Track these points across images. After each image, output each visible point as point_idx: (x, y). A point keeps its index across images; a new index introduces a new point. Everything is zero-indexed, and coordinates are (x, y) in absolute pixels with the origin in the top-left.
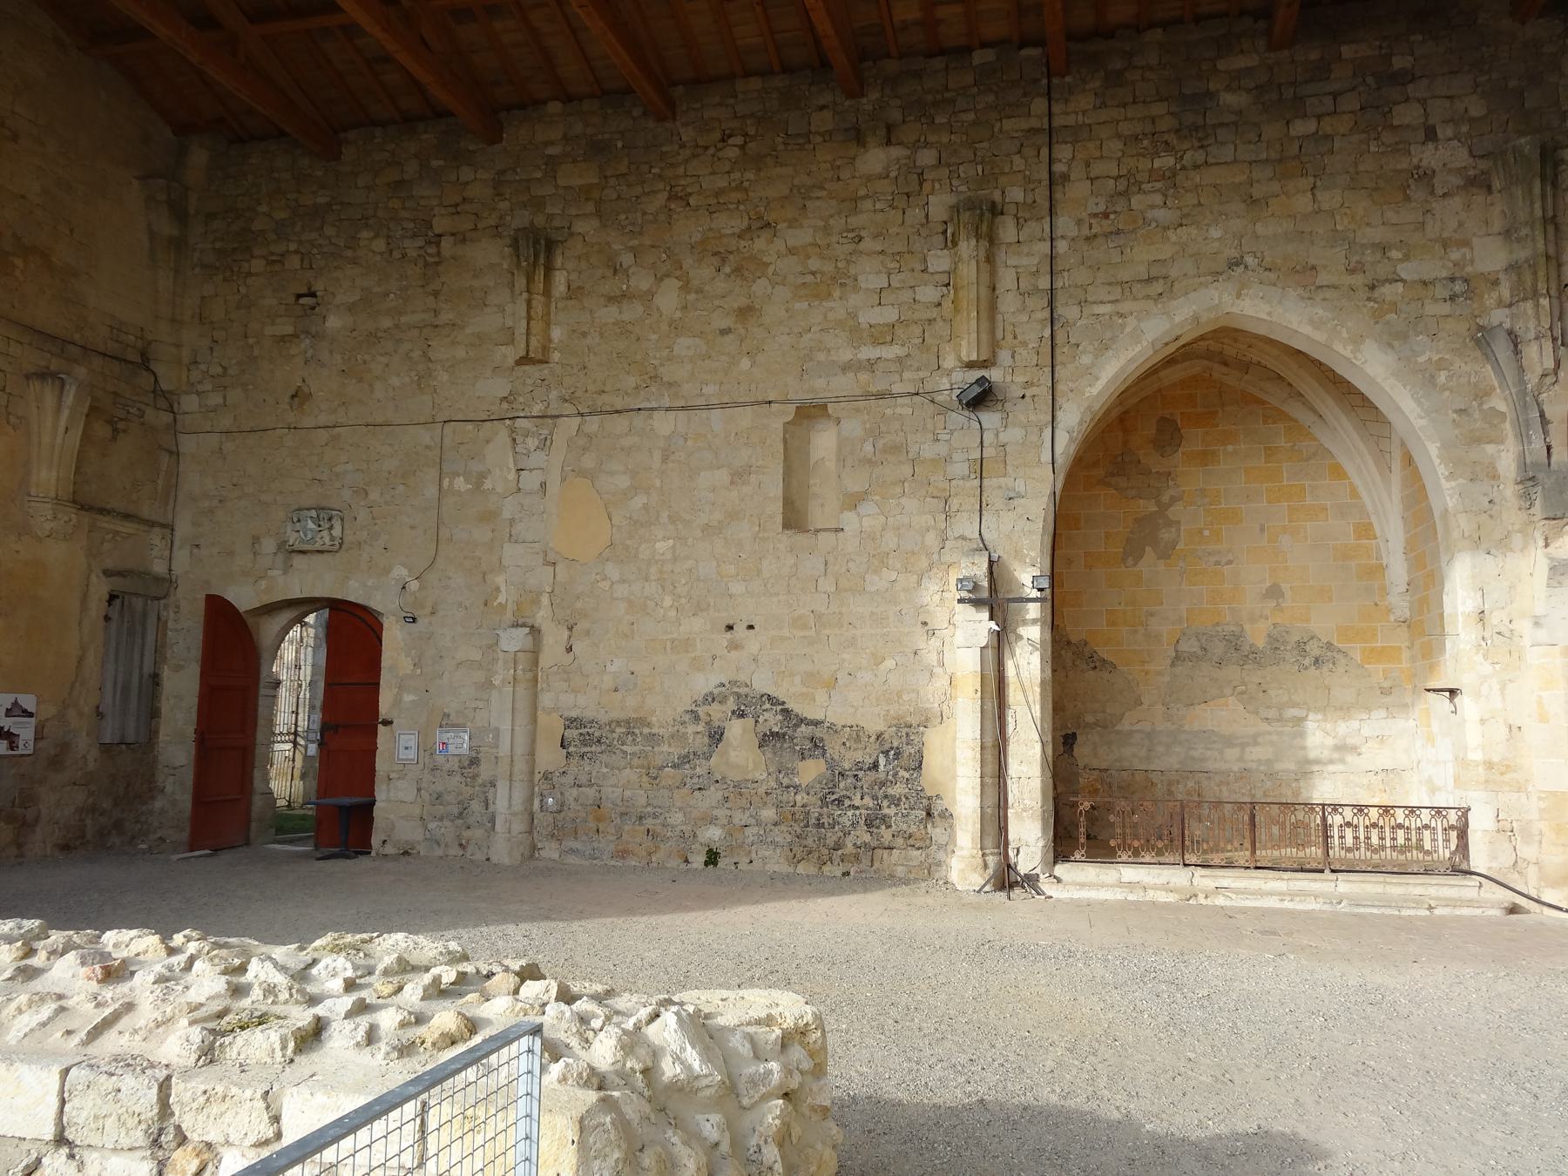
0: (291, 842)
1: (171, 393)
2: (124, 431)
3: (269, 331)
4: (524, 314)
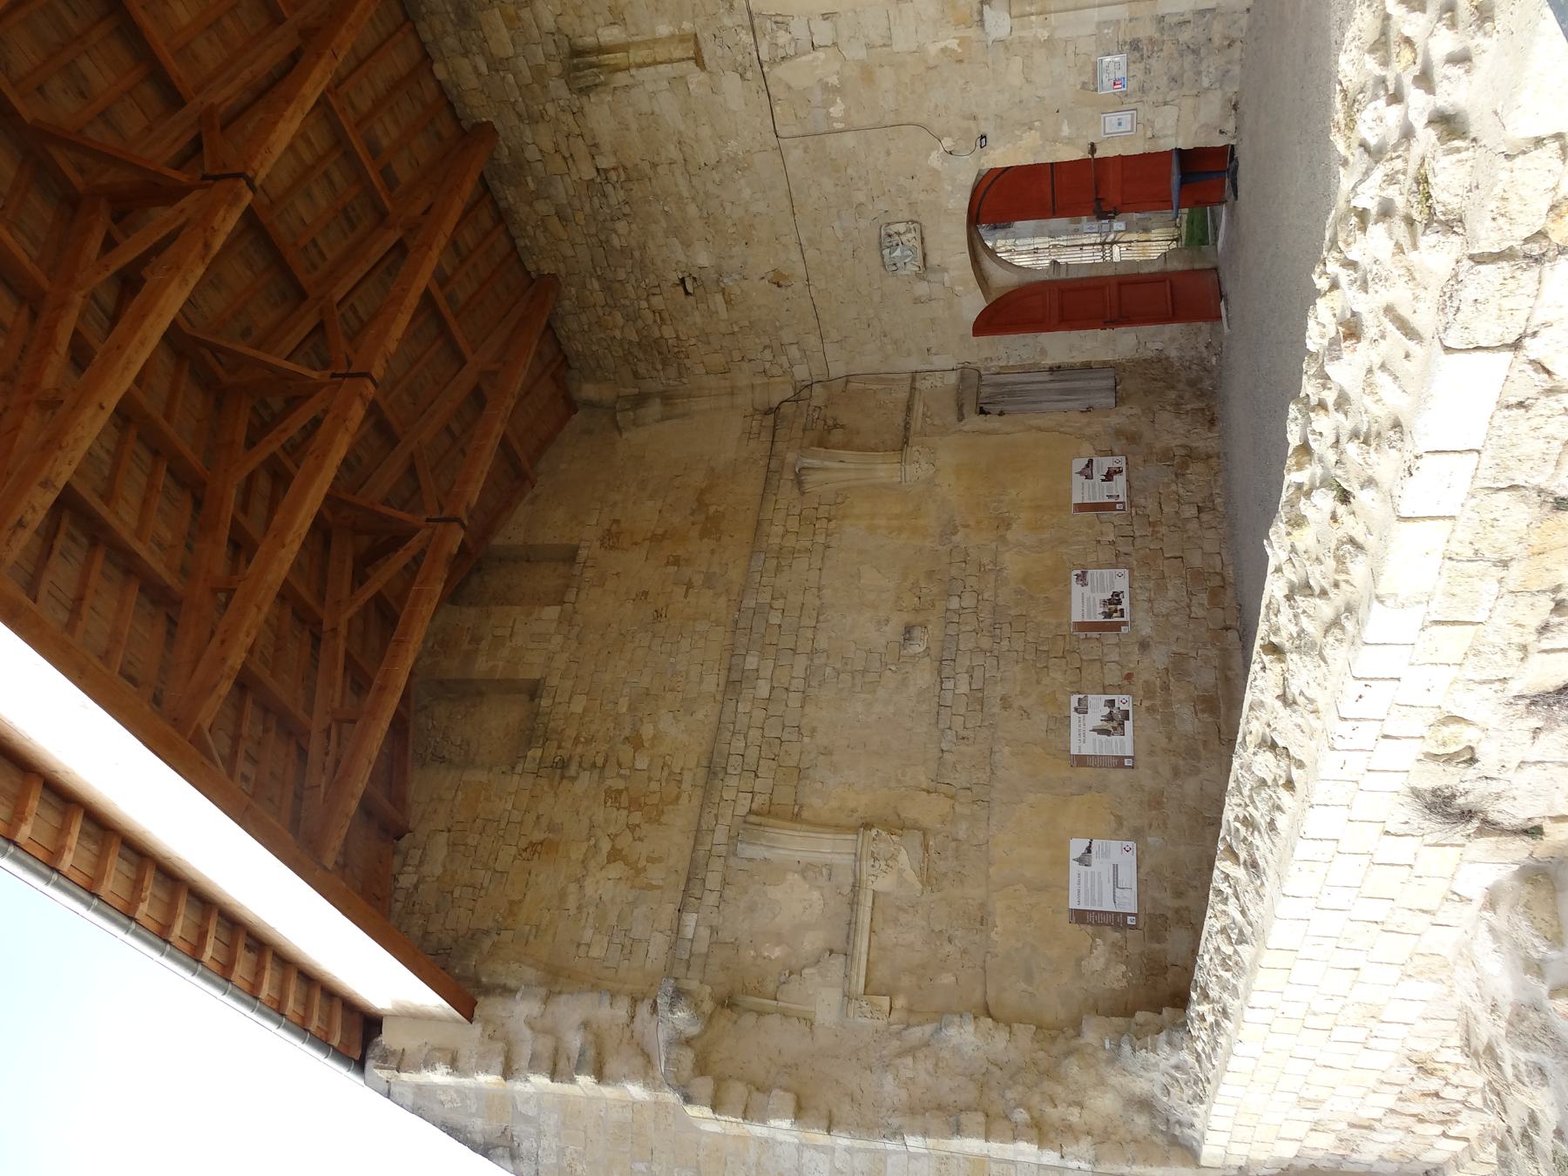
0: (1216, 229)
1: (795, 389)
2: (835, 420)
3: (724, 314)
4: (652, 70)
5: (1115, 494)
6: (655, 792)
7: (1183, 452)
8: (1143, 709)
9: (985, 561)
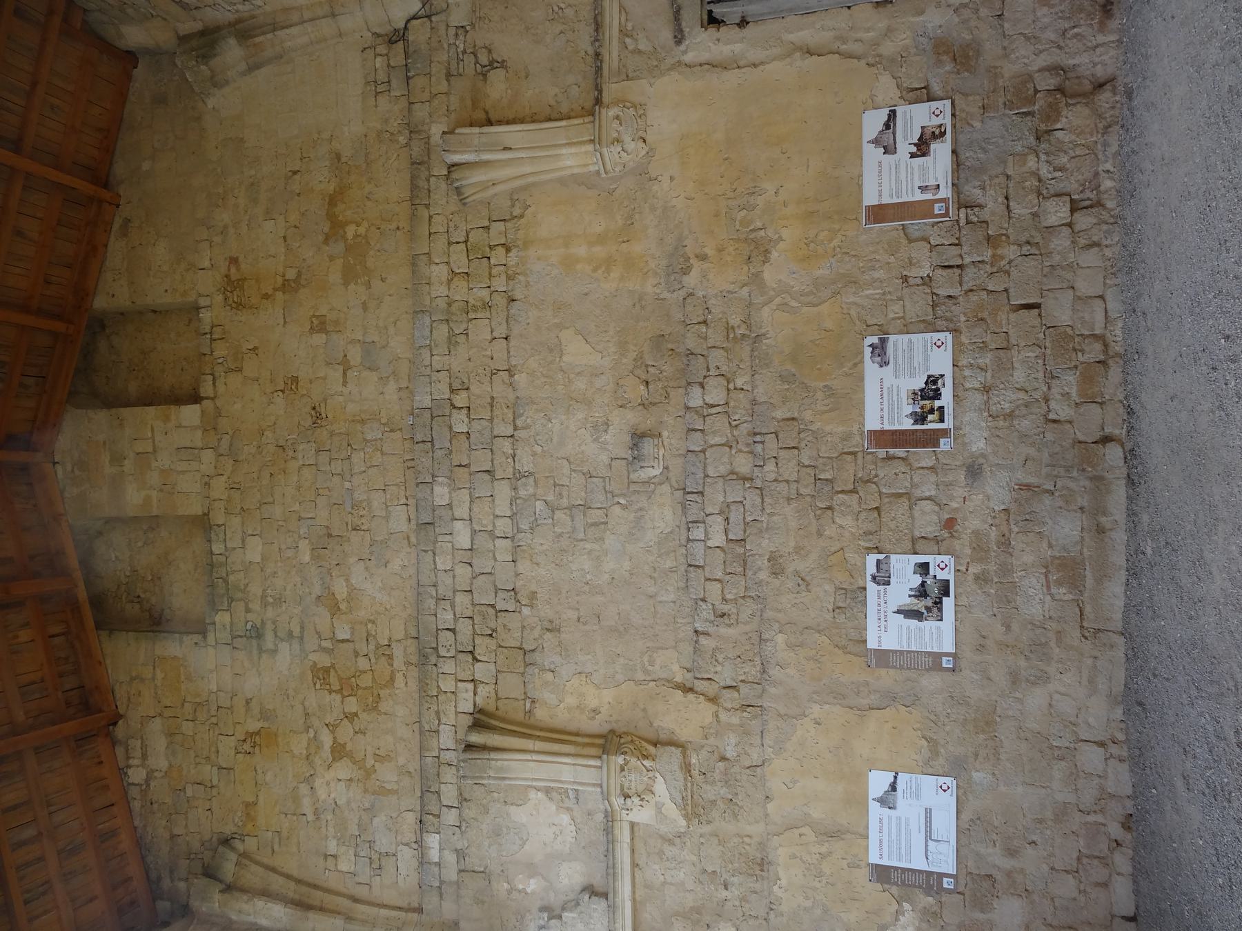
5: (932, 182)
6: (365, 672)
7: (1051, 82)
8: (970, 578)
9: (735, 320)
